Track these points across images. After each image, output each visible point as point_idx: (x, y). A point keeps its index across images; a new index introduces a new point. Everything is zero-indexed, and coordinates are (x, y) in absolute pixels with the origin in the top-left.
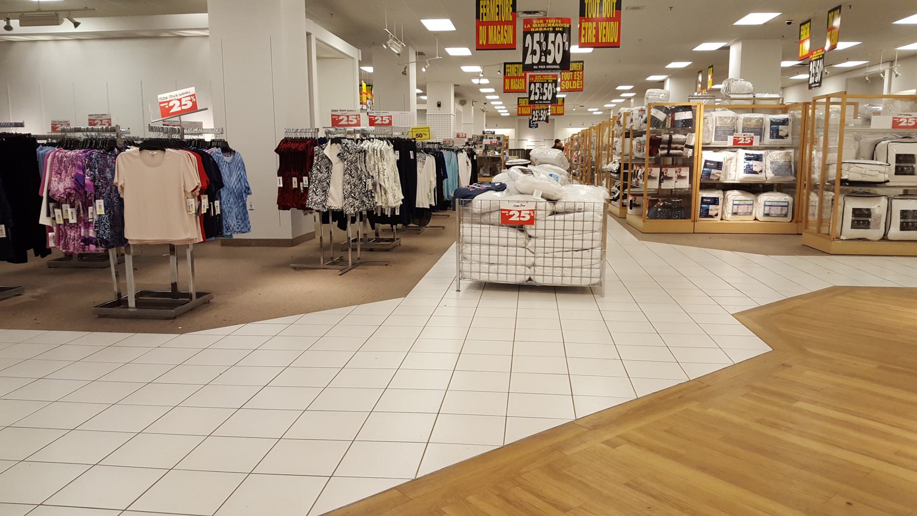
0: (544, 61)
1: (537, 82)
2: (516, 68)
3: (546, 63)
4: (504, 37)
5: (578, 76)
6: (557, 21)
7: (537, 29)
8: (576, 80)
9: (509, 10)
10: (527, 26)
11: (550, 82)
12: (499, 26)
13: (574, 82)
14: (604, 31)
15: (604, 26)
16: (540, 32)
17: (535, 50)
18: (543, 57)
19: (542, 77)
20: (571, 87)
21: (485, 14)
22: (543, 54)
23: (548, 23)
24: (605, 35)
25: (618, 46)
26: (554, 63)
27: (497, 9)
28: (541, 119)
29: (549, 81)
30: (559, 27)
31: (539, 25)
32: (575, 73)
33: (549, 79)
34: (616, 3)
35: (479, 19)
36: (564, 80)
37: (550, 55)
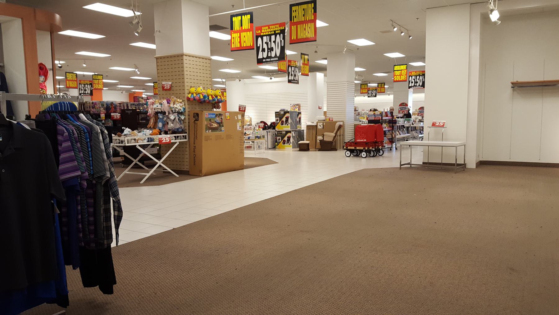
0: (270, 55)
1: (265, 36)
2: (304, 9)
3: (416, 86)
4: (308, 33)
5: (404, 72)
6: (276, 26)
7: (265, 34)
8: (403, 75)
9: (311, 11)
10: (258, 32)
11: (421, 75)
12: (304, 25)
13: (401, 76)
14: (244, 38)
15: (244, 35)
16: (414, 76)
17: (264, 49)
18: (269, 53)
19: (269, 28)
20: (400, 79)
21: (296, 16)
22: (269, 51)
23: (271, 28)
24: (245, 41)
25: (253, 48)
26: (276, 56)
27: (303, 11)
28: (418, 85)
29: (277, 32)
30: (278, 30)
31: (266, 31)
32: (99, 80)
33: (420, 73)
34: (250, 19)
35: (292, 21)
36: (396, 75)
37: (273, 51)
